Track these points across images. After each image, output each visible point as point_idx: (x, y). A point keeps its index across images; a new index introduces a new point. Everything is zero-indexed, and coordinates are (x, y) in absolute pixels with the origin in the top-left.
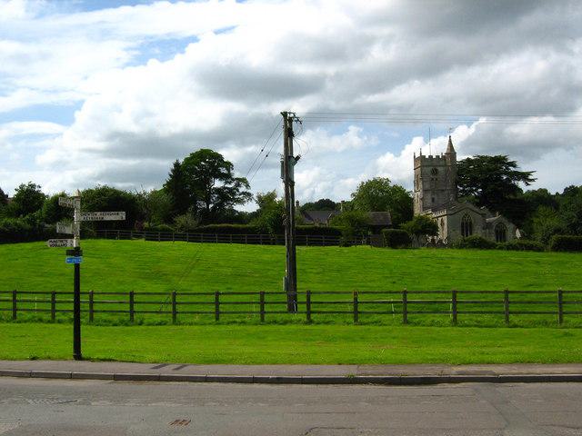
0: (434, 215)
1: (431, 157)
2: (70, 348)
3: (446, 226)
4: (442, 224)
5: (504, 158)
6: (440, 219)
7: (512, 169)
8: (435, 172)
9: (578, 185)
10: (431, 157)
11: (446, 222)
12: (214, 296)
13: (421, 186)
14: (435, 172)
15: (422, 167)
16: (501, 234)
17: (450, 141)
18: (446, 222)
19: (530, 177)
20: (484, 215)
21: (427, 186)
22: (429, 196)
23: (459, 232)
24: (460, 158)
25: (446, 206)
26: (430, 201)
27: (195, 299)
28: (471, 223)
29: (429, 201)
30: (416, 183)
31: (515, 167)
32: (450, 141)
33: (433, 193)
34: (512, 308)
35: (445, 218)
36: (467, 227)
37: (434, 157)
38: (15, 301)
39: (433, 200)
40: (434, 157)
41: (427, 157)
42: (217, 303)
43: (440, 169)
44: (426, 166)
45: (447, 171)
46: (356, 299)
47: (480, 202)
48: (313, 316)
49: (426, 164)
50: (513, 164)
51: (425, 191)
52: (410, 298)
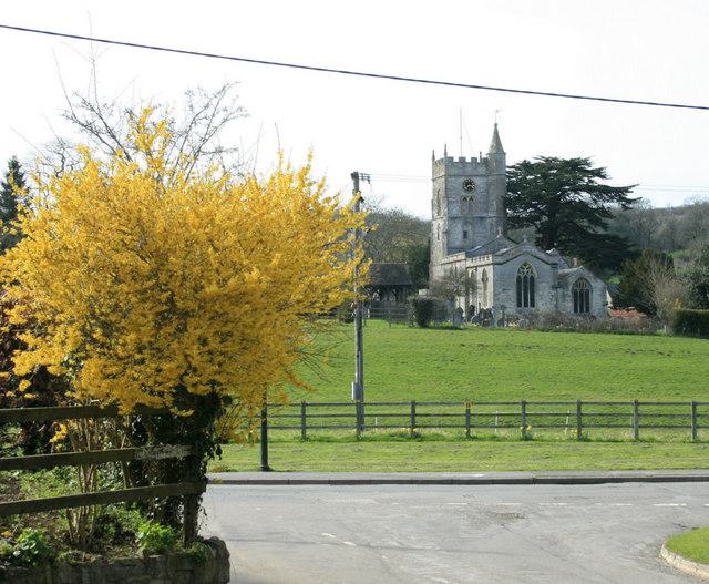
0: (469, 263)
1: (462, 160)
2: (258, 462)
3: (490, 283)
4: (484, 280)
5: (586, 162)
6: (480, 270)
7: (598, 181)
8: (469, 185)
9: (703, 197)
10: (462, 160)
11: (490, 275)
12: (300, 408)
13: (444, 210)
14: (469, 185)
15: (447, 176)
16: (582, 299)
17: (496, 133)
18: (490, 275)
19: (629, 196)
20: (554, 266)
21: (456, 211)
22: (458, 229)
23: (512, 293)
24: (513, 158)
25: (490, 249)
26: (460, 236)
27: (658, 421)
28: (532, 278)
29: (458, 240)
30: (436, 205)
31: (603, 177)
32: (496, 133)
33: (466, 223)
34: (643, 421)
35: (490, 270)
36: (526, 289)
37: (468, 160)
38: (304, 416)
39: (465, 234)
40: (468, 160)
41: (456, 160)
42: (304, 416)
43: (477, 181)
44: (458, 179)
45: (489, 185)
46: (468, 411)
47: (543, 244)
48: (308, 432)
49: (454, 171)
50: (599, 173)
51: (452, 219)
52: (474, 410)
